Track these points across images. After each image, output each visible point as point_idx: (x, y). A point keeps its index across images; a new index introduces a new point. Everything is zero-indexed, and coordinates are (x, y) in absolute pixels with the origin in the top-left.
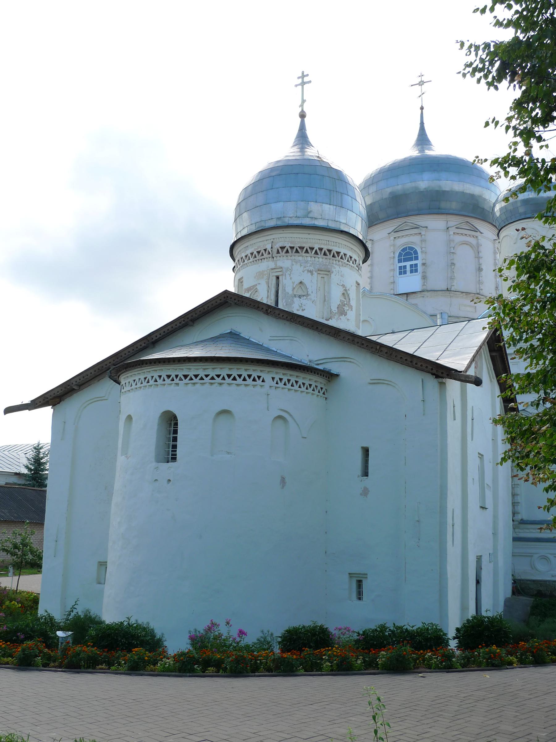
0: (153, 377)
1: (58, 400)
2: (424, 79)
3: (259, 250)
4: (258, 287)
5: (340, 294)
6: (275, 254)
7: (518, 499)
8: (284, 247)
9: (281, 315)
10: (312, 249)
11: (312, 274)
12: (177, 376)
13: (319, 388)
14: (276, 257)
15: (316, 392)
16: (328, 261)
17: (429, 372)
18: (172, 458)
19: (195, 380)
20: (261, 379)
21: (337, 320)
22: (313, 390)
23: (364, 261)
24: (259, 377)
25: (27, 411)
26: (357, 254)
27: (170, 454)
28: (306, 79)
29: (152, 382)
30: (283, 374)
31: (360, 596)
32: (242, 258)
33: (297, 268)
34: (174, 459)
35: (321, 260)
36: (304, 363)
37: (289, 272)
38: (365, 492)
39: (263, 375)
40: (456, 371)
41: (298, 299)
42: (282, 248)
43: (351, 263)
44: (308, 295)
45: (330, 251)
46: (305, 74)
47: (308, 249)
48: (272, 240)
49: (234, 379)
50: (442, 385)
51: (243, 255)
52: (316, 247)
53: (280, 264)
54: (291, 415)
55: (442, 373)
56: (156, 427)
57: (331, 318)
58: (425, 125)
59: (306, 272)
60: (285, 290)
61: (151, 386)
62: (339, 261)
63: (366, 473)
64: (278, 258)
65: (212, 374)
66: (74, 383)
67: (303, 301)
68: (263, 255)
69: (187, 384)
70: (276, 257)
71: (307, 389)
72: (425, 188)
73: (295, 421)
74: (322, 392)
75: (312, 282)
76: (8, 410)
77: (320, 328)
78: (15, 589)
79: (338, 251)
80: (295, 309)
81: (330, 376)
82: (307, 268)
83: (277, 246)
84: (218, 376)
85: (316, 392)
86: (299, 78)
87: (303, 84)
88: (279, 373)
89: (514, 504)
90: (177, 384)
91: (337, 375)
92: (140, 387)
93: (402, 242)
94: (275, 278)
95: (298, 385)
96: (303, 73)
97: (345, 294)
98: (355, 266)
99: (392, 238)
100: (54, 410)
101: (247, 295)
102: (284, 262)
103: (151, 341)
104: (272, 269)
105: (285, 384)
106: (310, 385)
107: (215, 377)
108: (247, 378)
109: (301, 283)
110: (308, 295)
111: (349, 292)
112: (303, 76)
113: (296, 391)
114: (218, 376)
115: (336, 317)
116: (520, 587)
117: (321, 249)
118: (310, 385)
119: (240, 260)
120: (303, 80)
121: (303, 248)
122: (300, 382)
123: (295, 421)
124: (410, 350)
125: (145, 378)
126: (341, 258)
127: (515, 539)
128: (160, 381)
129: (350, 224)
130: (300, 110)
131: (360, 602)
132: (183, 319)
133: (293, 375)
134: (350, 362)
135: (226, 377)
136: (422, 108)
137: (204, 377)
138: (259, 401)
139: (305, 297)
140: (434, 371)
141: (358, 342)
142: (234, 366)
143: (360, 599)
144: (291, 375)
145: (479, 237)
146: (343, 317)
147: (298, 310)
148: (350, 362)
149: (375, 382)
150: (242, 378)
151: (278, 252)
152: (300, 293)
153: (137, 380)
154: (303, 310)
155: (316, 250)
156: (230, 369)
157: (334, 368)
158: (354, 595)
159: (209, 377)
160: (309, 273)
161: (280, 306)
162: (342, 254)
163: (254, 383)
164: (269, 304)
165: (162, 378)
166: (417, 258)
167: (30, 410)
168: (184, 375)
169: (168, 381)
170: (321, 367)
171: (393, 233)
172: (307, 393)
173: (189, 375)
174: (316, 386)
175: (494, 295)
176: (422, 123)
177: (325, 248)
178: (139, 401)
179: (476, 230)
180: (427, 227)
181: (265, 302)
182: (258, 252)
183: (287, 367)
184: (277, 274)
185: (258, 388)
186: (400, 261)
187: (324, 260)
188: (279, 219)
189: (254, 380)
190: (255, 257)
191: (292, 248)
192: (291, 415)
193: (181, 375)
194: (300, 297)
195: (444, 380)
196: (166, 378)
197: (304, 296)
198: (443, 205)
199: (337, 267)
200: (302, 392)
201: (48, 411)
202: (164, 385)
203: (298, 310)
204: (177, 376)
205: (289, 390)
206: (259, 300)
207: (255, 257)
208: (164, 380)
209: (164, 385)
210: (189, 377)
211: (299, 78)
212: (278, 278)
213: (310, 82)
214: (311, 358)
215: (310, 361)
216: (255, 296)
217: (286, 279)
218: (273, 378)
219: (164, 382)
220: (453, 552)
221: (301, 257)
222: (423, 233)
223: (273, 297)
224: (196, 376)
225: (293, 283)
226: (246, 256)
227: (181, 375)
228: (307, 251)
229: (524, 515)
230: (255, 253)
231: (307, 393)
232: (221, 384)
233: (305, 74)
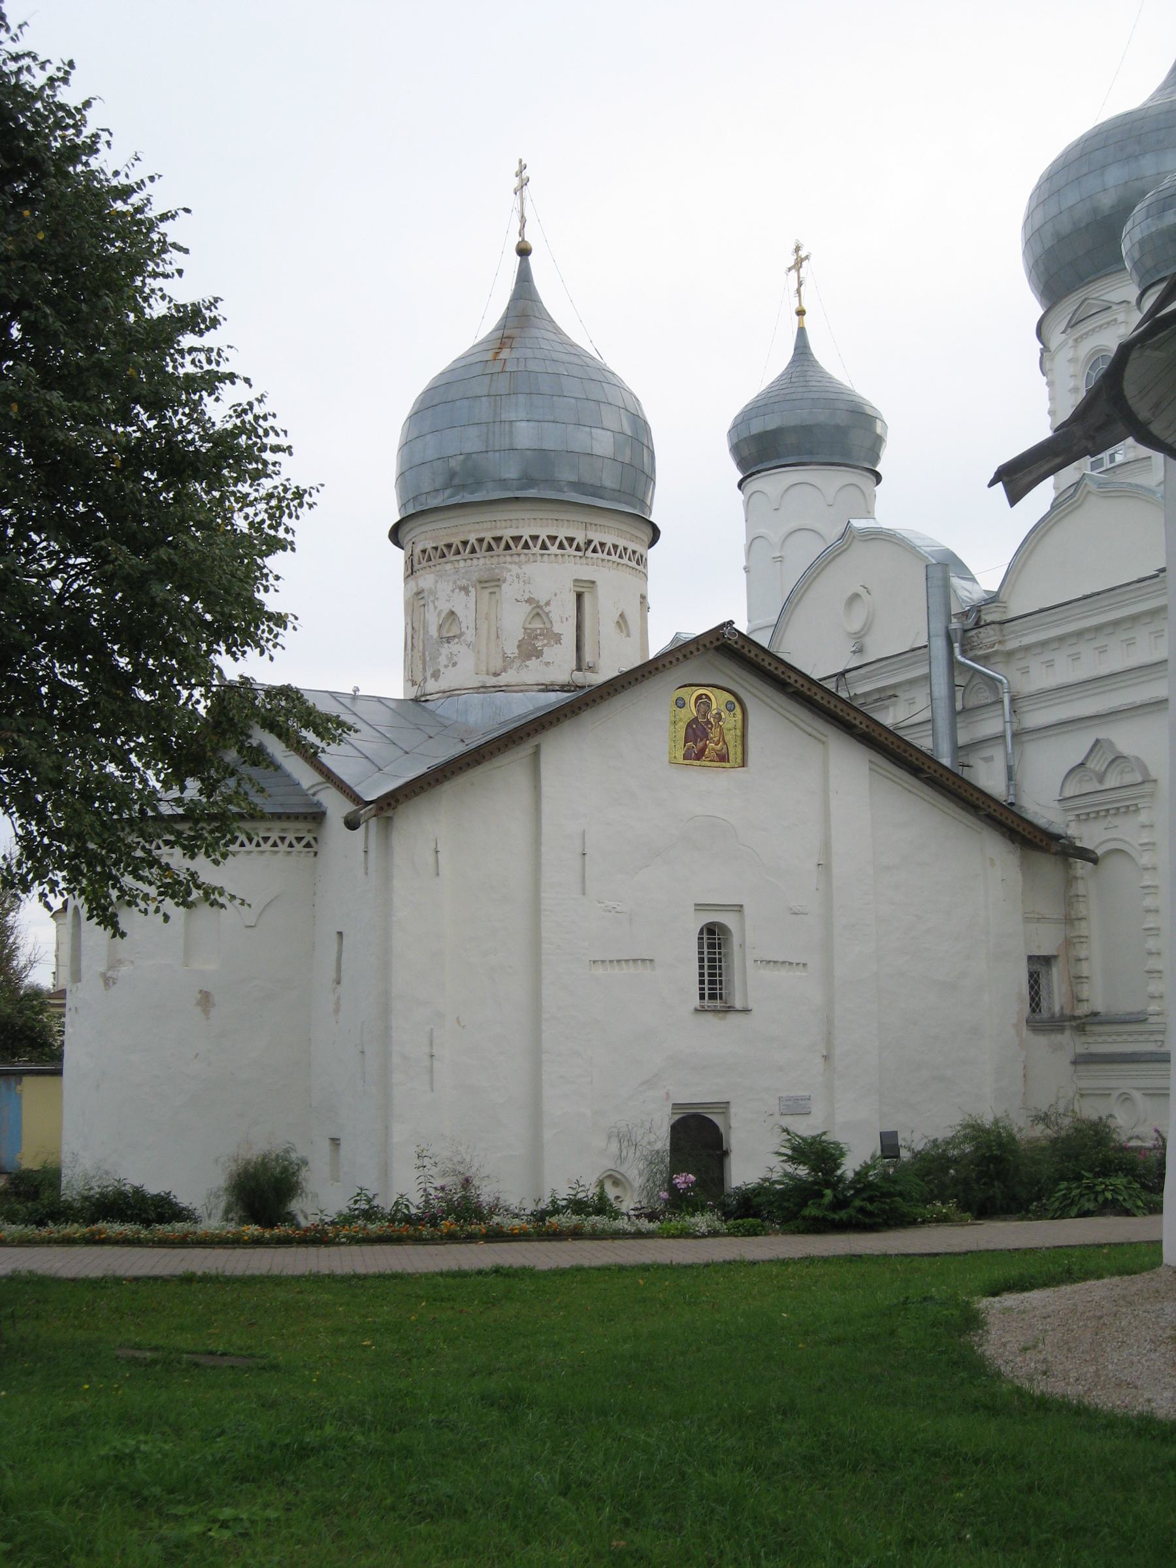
11: (467, 593)
16: (495, 560)
33: (444, 588)
35: (482, 563)
37: (432, 598)
41: (446, 645)
52: (472, 539)
62: (519, 555)
63: (338, 983)
72: (1113, 207)
77: (639, 676)
82: (459, 583)
110: (462, 634)
111: (547, 609)
115: (515, 666)
146: (533, 663)
172: (262, 852)
175: (542, 598)
177: (488, 536)
199: (515, 569)
225: (439, 615)
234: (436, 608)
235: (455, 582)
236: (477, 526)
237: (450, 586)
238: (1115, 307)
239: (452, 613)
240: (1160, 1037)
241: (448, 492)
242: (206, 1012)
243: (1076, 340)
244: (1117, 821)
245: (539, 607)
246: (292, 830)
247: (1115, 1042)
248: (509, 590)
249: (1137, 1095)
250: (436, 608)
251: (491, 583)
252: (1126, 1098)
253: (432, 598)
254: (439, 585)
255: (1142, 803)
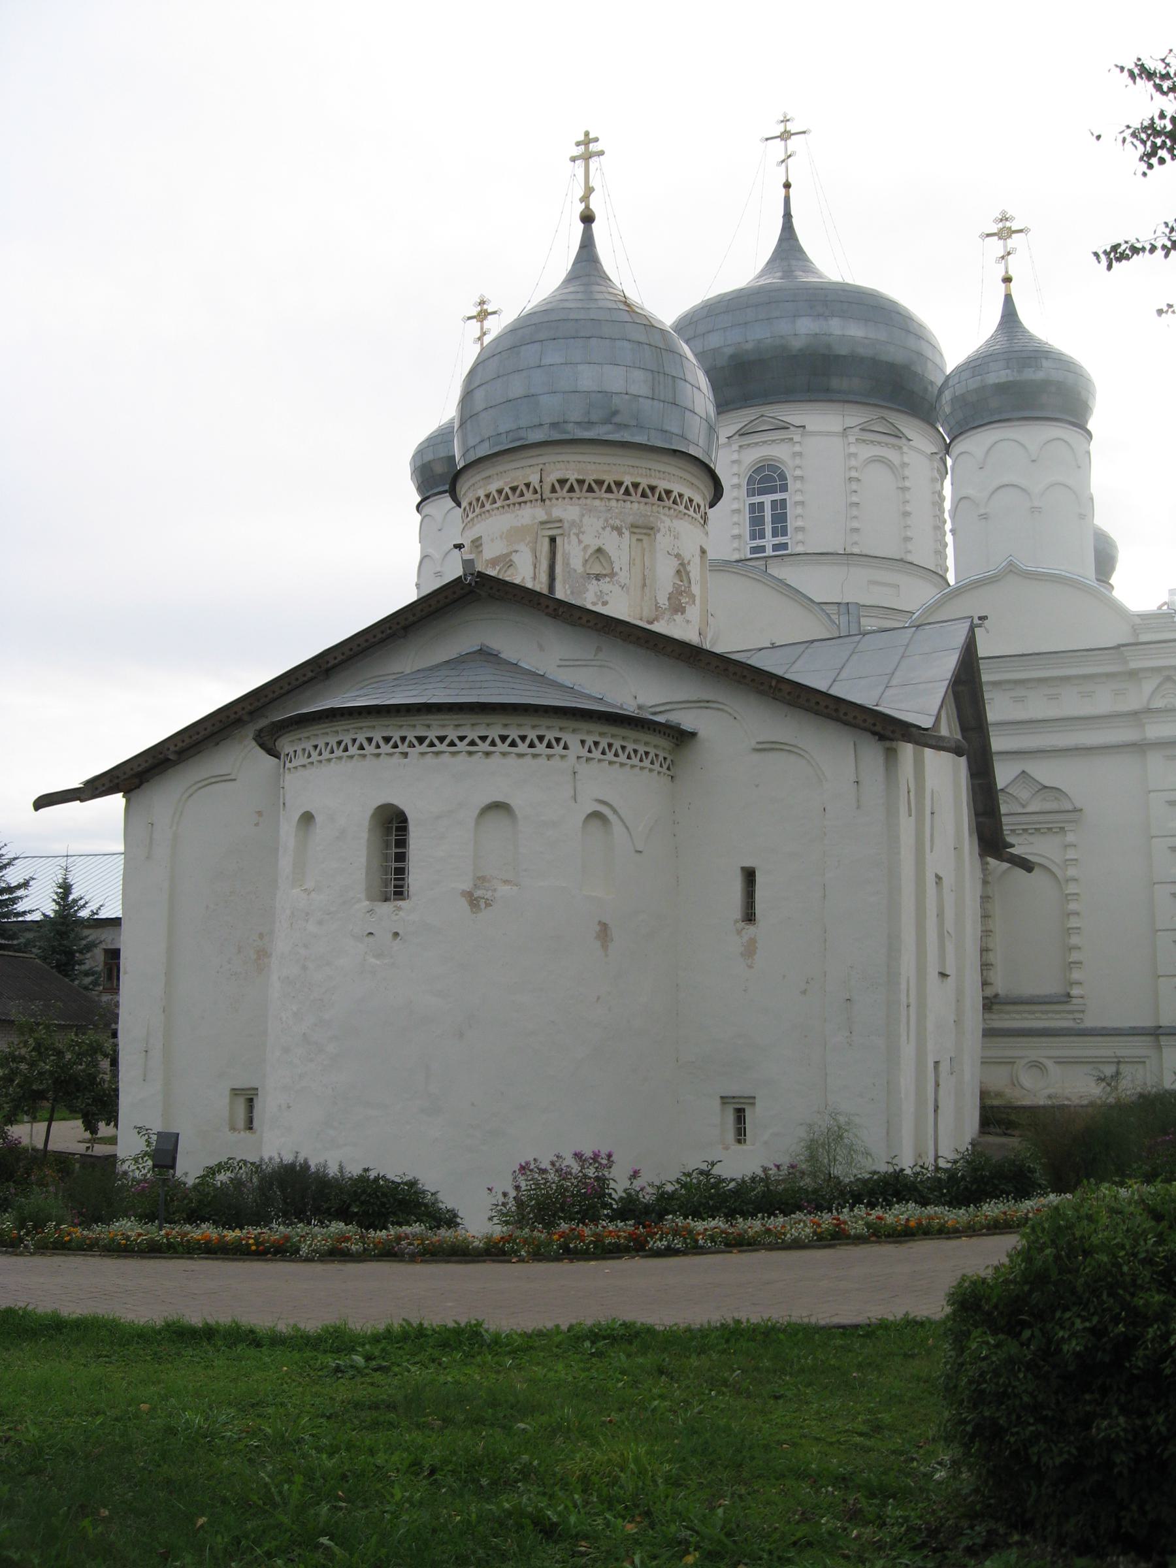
0: (354, 741)
1: (137, 781)
2: (792, 127)
3: (515, 484)
4: (515, 557)
5: (672, 572)
6: (547, 493)
7: (991, 957)
8: (567, 480)
9: (584, 620)
10: (619, 484)
12: (403, 739)
13: (661, 758)
14: (550, 499)
15: (657, 766)
16: (648, 508)
17: (865, 729)
18: (396, 893)
19: (440, 747)
20: (562, 744)
21: (668, 622)
22: (616, 755)
23: (712, 505)
24: (558, 740)
25: (77, 804)
26: (692, 489)
27: (393, 880)
28: (593, 147)
29: (353, 750)
30: (561, 729)
31: (741, 1134)
32: (478, 499)
34: (400, 893)
35: (635, 508)
36: (610, 705)
37: (575, 530)
38: (750, 950)
39: (566, 737)
40: (919, 727)
41: (594, 582)
42: (562, 482)
43: (691, 512)
44: (612, 575)
45: (653, 488)
46: (591, 136)
47: (613, 485)
48: (541, 466)
49: (513, 744)
50: (891, 755)
51: (481, 493)
52: (628, 481)
53: (557, 512)
54: (615, 811)
55: (893, 732)
56: (365, 835)
57: (656, 619)
58: (794, 220)
59: (609, 529)
60: (568, 564)
61: (352, 757)
62: (670, 508)
63: (749, 916)
64: (554, 501)
65: (472, 735)
66: (172, 748)
67: (605, 585)
68: (522, 495)
69: (423, 754)
70: (550, 499)
71: (641, 760)
72: (800, 350)
73: (622, 820)
74: (665, 766)
75: (619, 548)
76: (43, 802)
78: (41, 1146)
79: (668, 488)
80: (589, 601)
81: (681, 737)
83: (552, 478)
84: (483, 738)
85: (657, 766)
86: (578, 144)
87: (587, 157)
88: (593, 733)
89: (986, 966)
90: (405, 755)
91: (693, 735)
92: (329, 760)
93: (752, 456)
94: (546, 541)
95: (613, 750)
96: (587, 134)
97: (682, 572)
98: (698, 516)
99: (735, 447)
100: (128, 802)
101: (492, 572)
102: (566, 510)
103: (325, 667)
104: (542, 523)
105: (603, 753)
106: (647, 753)
107: (478, 741)
108: (536, 741)
109: (599, 550)
111: (689, 568)
112: (587, 140)
113: (622, 765)
114: (483, 738)
116: (995, 1117)
117: (636, 485)
118: (647, 753)
119: (474, 503)
120: (588, 150)
121: (603, 482)
122: (630, 749)
123: (622, 820)
124: (822, 686)
125: (339, 743)
126: (675, 502)
127: (989, 1033)
128: (370, 749)
129: (690, 437)
130: (583, 206)
131: (739, 1147)
132: (388, 625)
133: (617, 737)
134: (718, 709)
135: (498, 741)
136: (787, 186)
137: (457, 741)
138: (552, 786)
139: (608, 579)
140: (878, 728)
141: (735, 674)
142: (514, 720)
143: (739, 1141)
144: (613, 736)
145: (905, 449)
146: (678, 617)
147: (594, 604)
148: (718, 709)
149: (764, 748)
150: (528, 741)
151: (553, 490)
152: (597, 569)
153: (321, 745)
154: (605, 603)
155: (627, 488)
156: (506, 725)
157: (687, 720)
158: (731, 1135)
159: (467, 741)
160: (615, 533)
161: (560, 594)
162: (675, 493)
163: (549, 751)
164: (538, 590)
165: (374, 743)
166: (784, 488)
167: (82, 801)
168: (438, 737)
169: (386, 748)
170: (660, 719)
171: (737, 437)
172: (642, 768)
173: (426, 737)
174: (656, 755)
176: (788, 216)
177: (644, 482)
178: (339, 789)
179: (898, 435)
180: (804, 427)
181: (529, 585)
182: (514, 489)
183: (556, 713)
184: (551, 533)
185: (555, 762)
186: (751, 493)
187: (642, 506)
188: (554, 425)
189: (549, 746)
190: (507, 498)
191: (581, 482)
192: (615, 811)
193: (411, 737)
194: (598, 577)
195: (894, 744)
196: (381, 743)
197: (605, 575)
198: (835, 383)
200: (633, 766)
201: (117, 801)
202: (378, 755)
203: (594, 604)
204: (403, 739)
205: (611, 763)
206: (517, 582)
207: (507, 498)
208: (378, 747)
209: (378, 755)
210: (427, 742)
211: (578, 144)
212: (553, 540)
213: (601, 153)
214: (640, 701)
215: (640, 707)
216: (509, 573)
217: (569, 543)
218: (583, 742)
219: (378, 751)
220: (908, 1051)
221: (596, 502)
222: (797, 438)
223: (544, 577)
224: (441, 739)
225: (586, 548)
226: (488, 496)
227: (411, 737)
228: (609, 490)
229: (1000, 986)
230: (507, 489)
231: (642, 768)
232: (487, 754)
233: (591, 136)
234: (580, 542)
235: (606, 520)
236: (632, 470)
237: (601, 523)
238: (792, 428)
239: (599, 550)
240: (1077, 1015)
241: (609, 427)
242: (605, 947)
243: (740, 447)
244: (1031, 839)
245: (682, 564)
246: (658, 745)
247: (1014, 1019)
248: (663, 541)
249: (1049, 1064)
250: (580, 542)
251: (644, 530)
252: (1037, 1065)
253: (575, 530)
254: (586, 520)
255: (1068, 827)
